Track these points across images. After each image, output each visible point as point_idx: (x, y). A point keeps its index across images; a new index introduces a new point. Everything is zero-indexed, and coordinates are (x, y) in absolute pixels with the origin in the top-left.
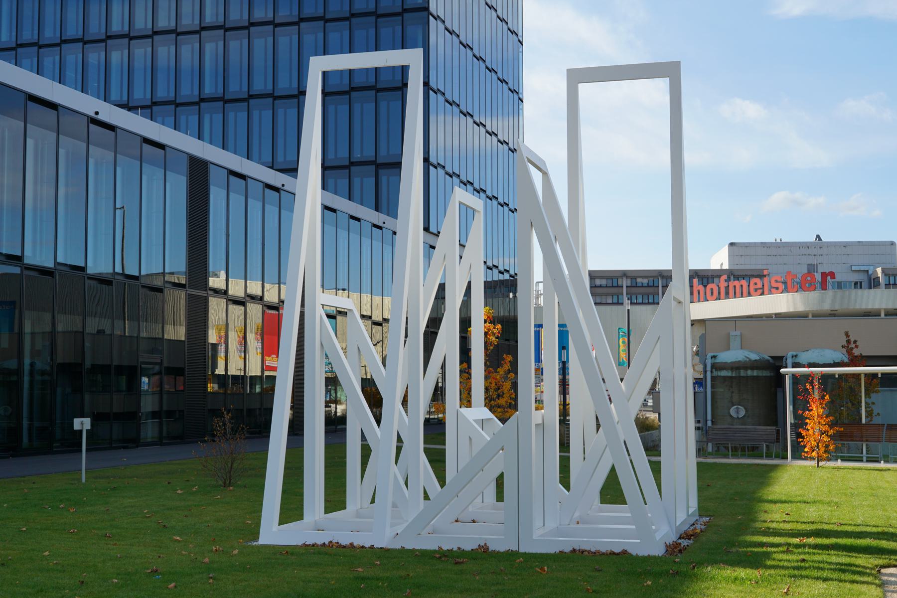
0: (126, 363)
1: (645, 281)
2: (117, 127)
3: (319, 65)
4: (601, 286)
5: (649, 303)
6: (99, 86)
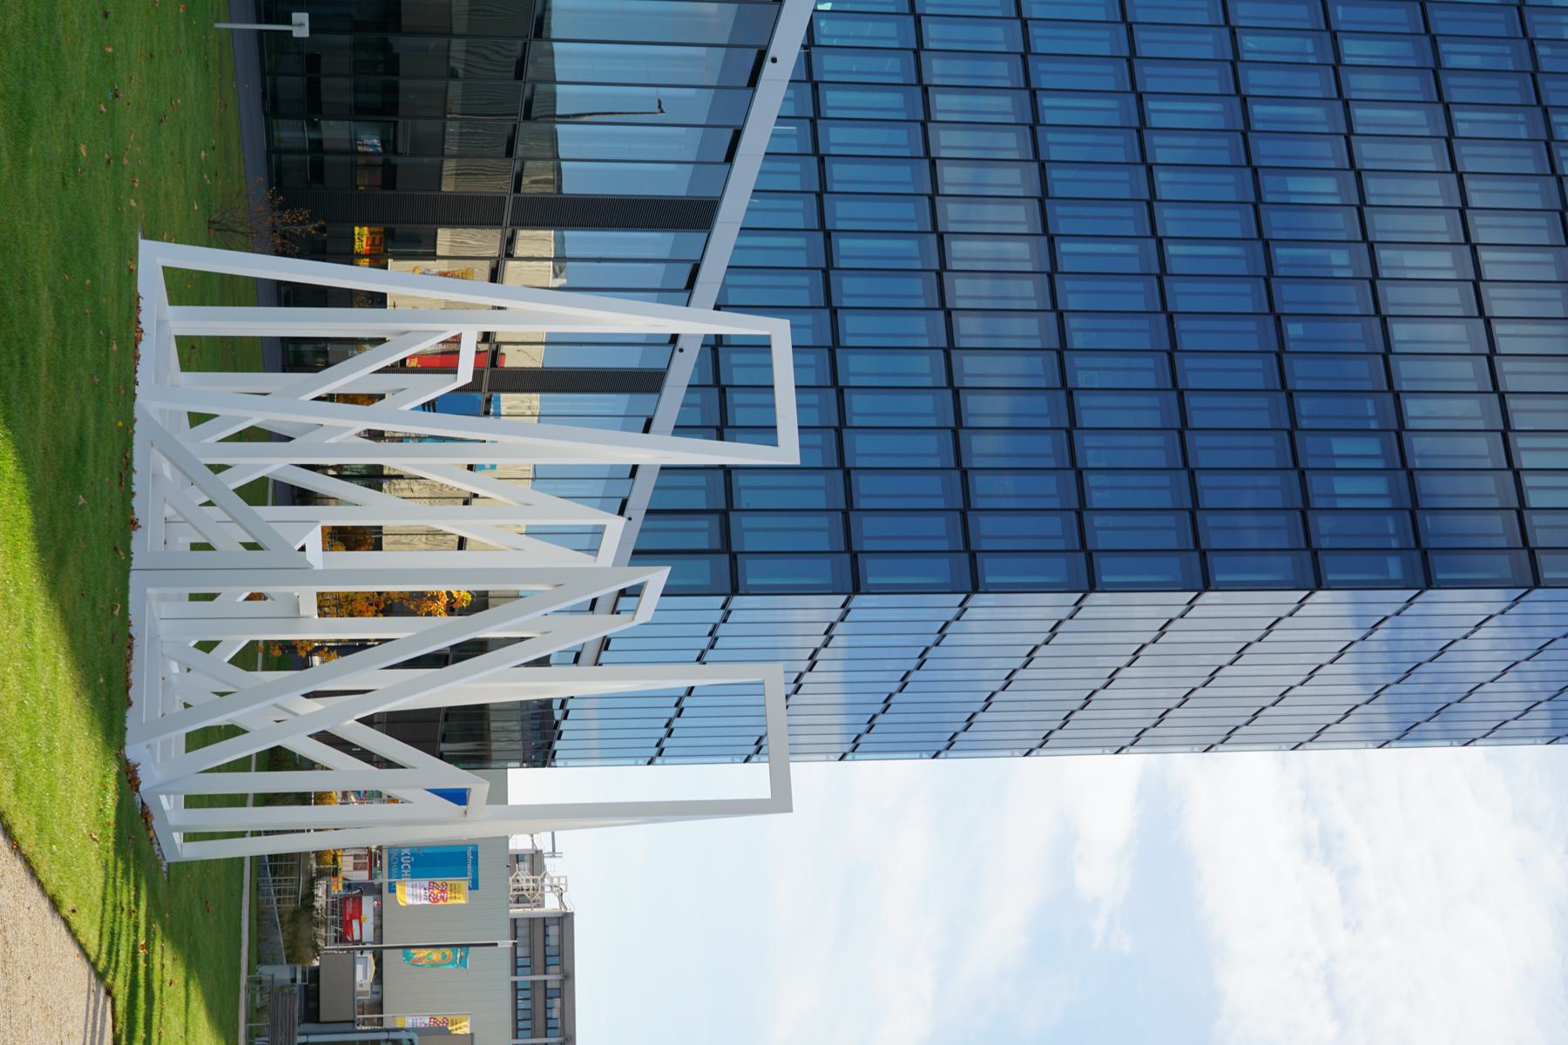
0: (402, 99)
1: (555, 1013)
2: (755, 91)
3: (779, 331)
4: (546, 935)
5: (516, 1021)
6: (852, 73)
